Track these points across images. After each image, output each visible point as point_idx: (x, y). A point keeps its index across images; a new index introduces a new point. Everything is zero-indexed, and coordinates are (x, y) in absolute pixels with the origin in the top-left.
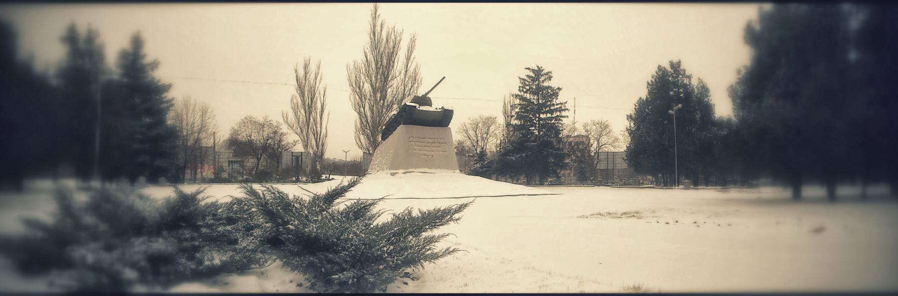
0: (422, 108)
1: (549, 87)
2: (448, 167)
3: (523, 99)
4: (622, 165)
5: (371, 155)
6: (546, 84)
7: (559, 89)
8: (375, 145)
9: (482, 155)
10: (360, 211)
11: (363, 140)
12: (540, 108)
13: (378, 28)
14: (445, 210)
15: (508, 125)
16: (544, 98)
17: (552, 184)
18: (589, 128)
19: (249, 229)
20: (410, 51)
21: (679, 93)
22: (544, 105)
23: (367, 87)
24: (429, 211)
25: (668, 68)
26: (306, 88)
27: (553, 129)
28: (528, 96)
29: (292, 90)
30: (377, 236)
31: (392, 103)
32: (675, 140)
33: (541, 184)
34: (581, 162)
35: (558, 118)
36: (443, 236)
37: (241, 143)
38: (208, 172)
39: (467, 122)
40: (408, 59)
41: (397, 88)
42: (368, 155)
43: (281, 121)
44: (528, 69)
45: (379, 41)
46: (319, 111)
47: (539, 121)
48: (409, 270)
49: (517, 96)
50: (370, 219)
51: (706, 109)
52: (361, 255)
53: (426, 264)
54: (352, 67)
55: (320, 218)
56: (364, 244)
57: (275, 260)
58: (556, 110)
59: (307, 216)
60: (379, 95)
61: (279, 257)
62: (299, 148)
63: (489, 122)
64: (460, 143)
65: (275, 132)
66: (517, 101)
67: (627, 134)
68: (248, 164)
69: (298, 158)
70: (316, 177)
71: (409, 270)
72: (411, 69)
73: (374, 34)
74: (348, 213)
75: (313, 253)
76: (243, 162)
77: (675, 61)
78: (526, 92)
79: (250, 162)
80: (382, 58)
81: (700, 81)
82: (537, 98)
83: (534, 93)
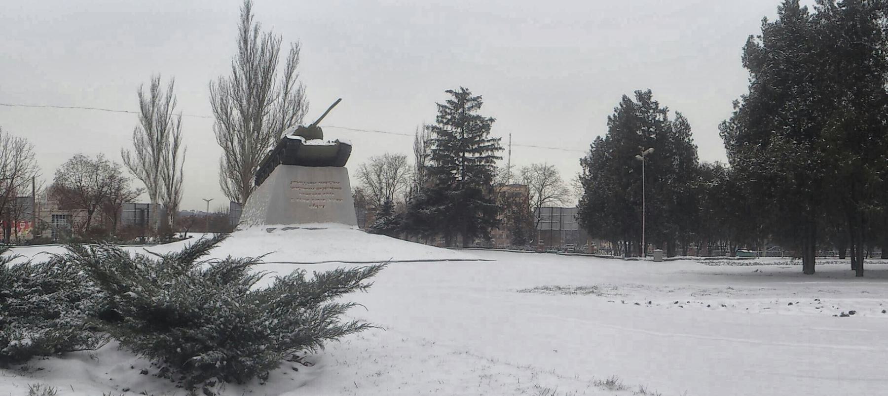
0: (309, 143)
1: (478, 117)
3: (441, 132)
5: (241, 205)
6: (473, 113)
8: (246, 192)
9: (388, 205)
10: (231, 272)
12: (464, 145)
13: (251, 34)
14: (349, 272)
15: (421, 167)
16: (470, 131)
17: (479, 247)
18: (529, 174)
19: (73, 300)
20: (292, 65)
21: (650, 133)
22: (471, 141)
23: (236, 114)
24: (328, 273)
25: (634, 100)
26: (155, 117)
27: (482, 173)
28: (449, 128)
29: (135, 120)
31: (268, 136)
32: (644, 196)
33: (466, 246)
35: (489, 159)
36: (348, 306)
37: (69, 191)
38: (25, 232)
39: (369, 163)
40: (288, 77)
42: (237, 206)
43: (120, 161)
44: (450, 92)
45: (252, 49)
46: (171, 147)
48: (300, 353)
49: (434, 128)
51: (689, 151)
52: (233, 329)
53: (327, 343)
54: (217, 86)
55: (174, 282)
56: (238, 316)
57: (108, 340)
58: (487, 148)
59: (154, 281)
60: (252, 124)
61: (114, 335)
62: (145, 199)
63: (396, 162)
64: (359, 191)
65: (112, 177)
66: (434, 136)
67: (580, 184)
68: (78, 219)
69: (143, 212)
70: (167, 237)
71: (300, 353)
72: (293, 91)
73: (246, 42)
75: (165, 329)
77: (644, 90)
78: (447, 123)
79: (80, 216)
80: (256, 74)
81: (679, 115)
82: (462, 131)
83: (456, 125)
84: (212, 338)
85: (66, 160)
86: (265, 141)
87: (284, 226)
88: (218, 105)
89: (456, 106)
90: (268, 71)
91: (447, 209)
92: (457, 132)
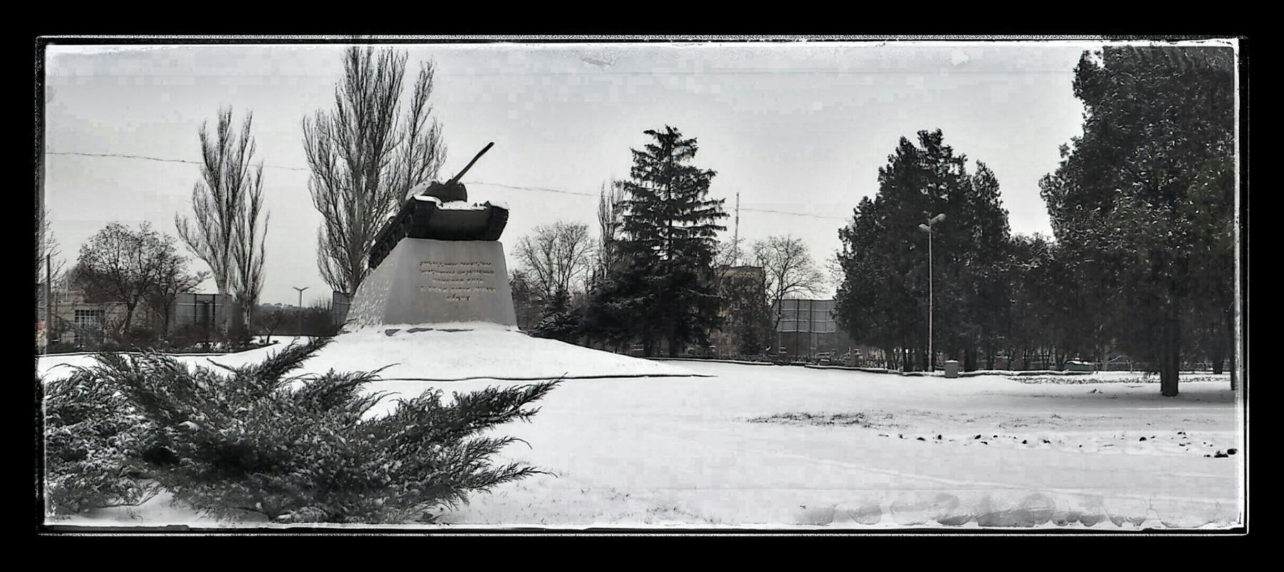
0: (447, 206)
2: (501, 320)
3: (637, 191)
4: (826, 325)
5: (349, 297)
6: (684, 163)
7: (711, 173)
8: (356, 277)
9: (562, 295)
10: (335, 393)
11: (333, 269)
14: (505, 393)
15: (609, 241)
16: (680, 189)
17: (692, 357)
18: (764, 252)
20: (422, 94)
21: (940, 192)
22: (682, 204)
23: (341, 165)
24: (475, 394)
25: (917, 144)
26: (224, 169)
27: (696, 250)
28: (649, 185)
29: (195, 173)
30: (372, 441)
31: (388, 196)
33: (674, 354)
34: (748, 318)
35: (708, 230)
37: (100, 275)
39: (533, 236)
40: (417, 111)
41: (397, 168)
42: (343, 298)
43: (174, 233)
44: (651, 132)
45: (365, 72)
46: (247, 212)
47: (670, 233)
49: (627, 185)
50: (356, 408)
51: (997, 219)
53: (473, 495)
54: (313, 124)
55: (251, 408)
57: (156, 491)
58: (704, 214)
59: (223, 407)
60: (364, 180)
61: (164, 484)
62: (209, 287)
63: (572, 235)
64: (519, 276)
65: (162, 256)
66: (628, 196)
67: (838, 266)
68: (112, 317)
69: (206, 305)
70: (241, 342)
72: (424, 132)
74: (308, 397)
76: (103, 312)
77: (931, 130)
78: (646, 178)
79: (116, 312)
80: (370, 107)
81: (982, 167)
83: (661, 181)
84: (306, 488)
85: (95, 232)
86: (383, 204)
87: (410, 327)
88: (315, 151)
89: (660, 154)
90: (388, 102)
91: (646, 302)
92: (660, 190)
